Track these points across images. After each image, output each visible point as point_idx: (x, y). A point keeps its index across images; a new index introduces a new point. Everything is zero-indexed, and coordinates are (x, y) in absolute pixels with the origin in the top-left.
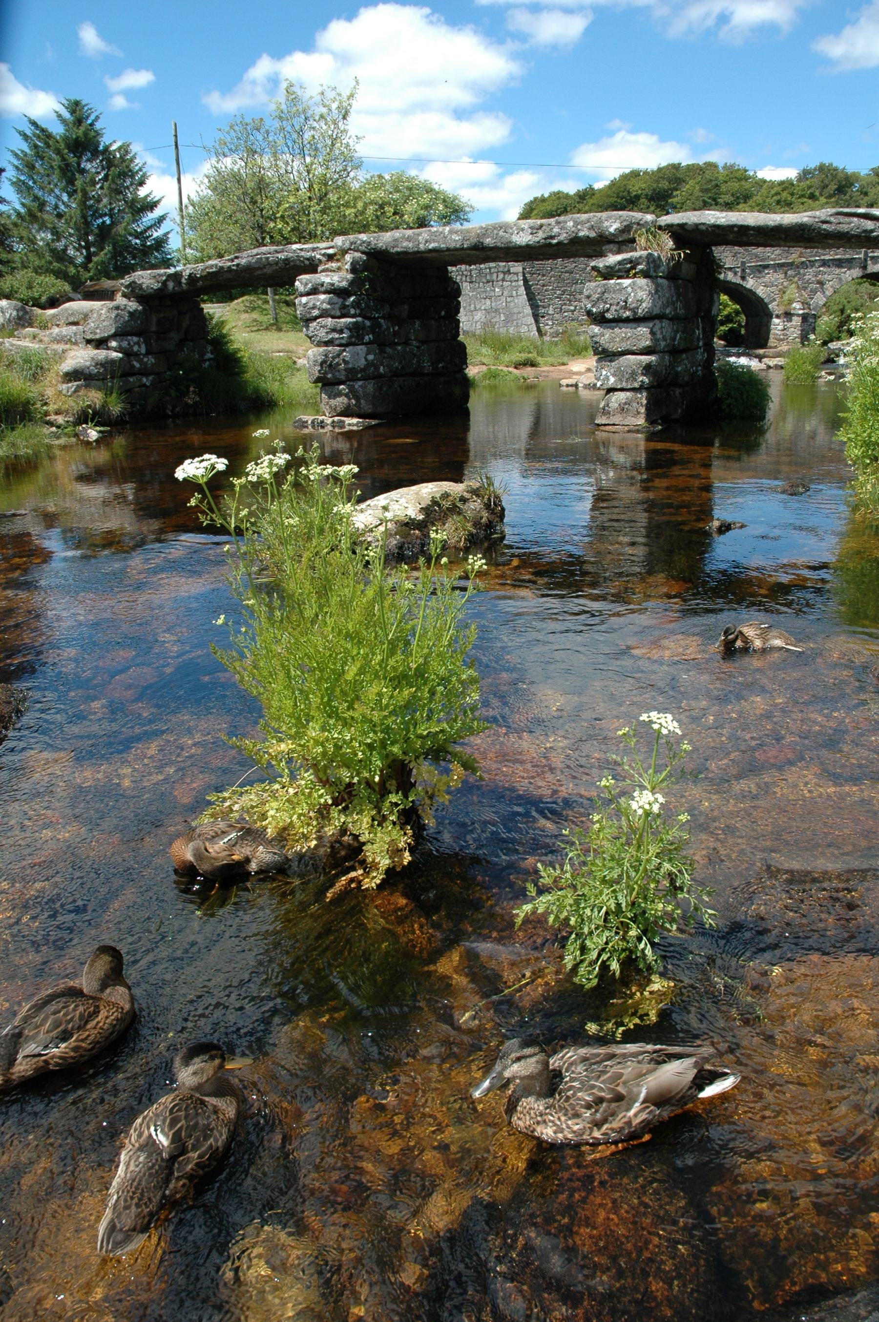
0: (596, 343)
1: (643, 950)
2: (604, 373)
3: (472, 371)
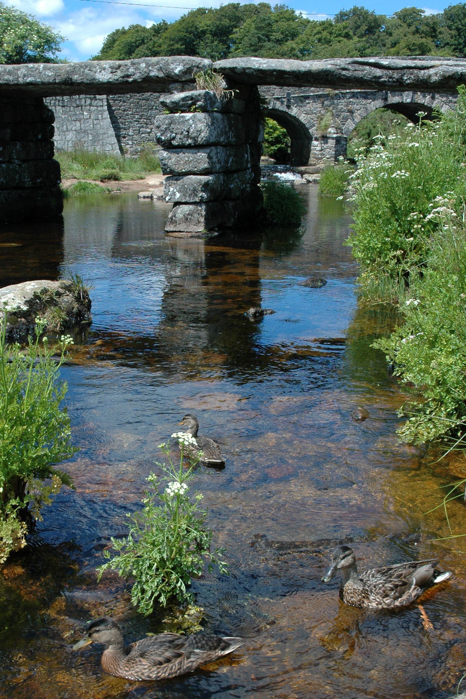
0: (165, 165)
1: (180, 587)
2: (171, 189)
3: (66, 184)
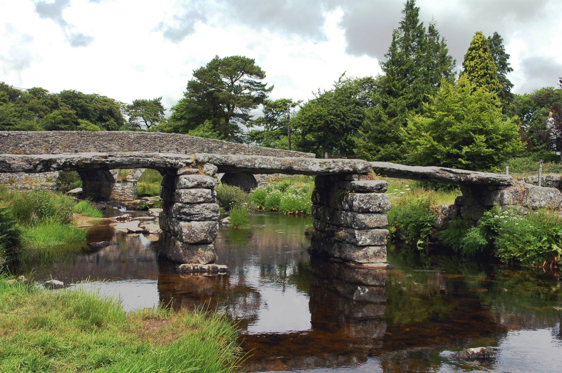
2: (363, 237)
